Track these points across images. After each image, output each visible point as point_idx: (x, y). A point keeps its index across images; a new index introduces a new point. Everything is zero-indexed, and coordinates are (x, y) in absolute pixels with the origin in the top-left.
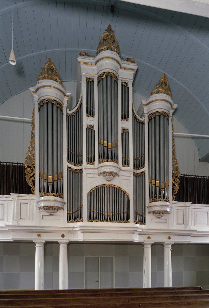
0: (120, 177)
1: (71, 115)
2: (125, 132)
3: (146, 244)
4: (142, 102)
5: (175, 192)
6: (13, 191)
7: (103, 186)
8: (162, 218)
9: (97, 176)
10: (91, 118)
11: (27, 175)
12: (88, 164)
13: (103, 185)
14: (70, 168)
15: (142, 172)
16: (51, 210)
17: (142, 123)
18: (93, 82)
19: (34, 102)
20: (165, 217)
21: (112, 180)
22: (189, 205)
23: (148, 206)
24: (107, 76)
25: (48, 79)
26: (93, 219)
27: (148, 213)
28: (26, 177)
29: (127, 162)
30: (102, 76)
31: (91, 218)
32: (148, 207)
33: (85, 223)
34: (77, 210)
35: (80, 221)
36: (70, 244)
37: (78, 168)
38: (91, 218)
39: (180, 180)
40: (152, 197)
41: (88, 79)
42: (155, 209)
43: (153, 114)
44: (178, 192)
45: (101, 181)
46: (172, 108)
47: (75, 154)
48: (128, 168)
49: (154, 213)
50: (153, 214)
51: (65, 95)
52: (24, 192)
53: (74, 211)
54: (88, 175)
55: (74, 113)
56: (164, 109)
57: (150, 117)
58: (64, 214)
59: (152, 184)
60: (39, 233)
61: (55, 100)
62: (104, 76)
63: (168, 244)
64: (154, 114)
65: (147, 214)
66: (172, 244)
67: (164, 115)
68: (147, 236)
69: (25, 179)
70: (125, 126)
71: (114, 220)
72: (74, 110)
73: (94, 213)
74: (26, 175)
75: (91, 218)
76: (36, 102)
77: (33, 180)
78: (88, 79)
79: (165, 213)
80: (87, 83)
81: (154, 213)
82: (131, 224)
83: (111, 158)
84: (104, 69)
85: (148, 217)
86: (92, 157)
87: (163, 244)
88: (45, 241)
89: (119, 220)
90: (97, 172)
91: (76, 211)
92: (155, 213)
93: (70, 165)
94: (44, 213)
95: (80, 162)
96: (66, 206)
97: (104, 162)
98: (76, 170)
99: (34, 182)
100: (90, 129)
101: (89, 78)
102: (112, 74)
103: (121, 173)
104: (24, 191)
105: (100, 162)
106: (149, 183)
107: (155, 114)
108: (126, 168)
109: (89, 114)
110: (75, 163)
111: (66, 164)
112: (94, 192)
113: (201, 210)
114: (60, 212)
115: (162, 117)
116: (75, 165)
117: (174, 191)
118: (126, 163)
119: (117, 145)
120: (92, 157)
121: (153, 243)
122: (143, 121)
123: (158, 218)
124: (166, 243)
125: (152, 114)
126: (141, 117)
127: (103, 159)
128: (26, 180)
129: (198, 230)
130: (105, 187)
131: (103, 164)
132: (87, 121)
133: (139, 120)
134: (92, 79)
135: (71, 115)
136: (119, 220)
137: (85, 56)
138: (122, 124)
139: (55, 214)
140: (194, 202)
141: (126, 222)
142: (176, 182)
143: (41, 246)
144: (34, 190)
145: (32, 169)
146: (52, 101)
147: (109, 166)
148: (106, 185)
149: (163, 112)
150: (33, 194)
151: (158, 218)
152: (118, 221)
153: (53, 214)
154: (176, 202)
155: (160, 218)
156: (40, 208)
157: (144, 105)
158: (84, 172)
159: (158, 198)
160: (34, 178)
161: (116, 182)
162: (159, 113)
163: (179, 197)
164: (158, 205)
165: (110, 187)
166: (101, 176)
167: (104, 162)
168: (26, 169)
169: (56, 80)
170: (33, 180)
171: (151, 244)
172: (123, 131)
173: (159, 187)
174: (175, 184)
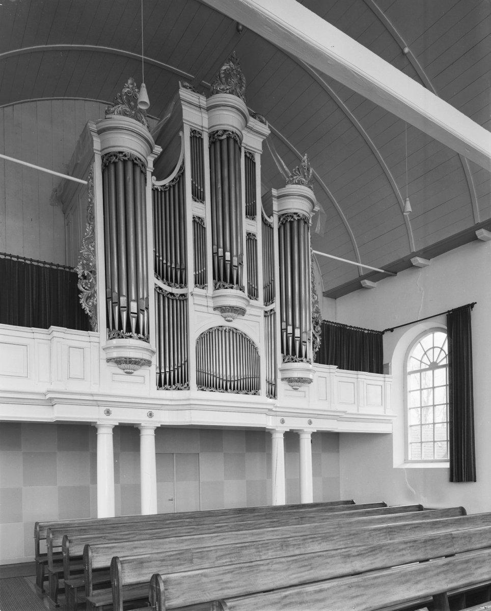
0: (246, 317)
1: (160, 190)
2: (251, 239)
3: (103, 426)
4: (89, 124)
5: (316, 348)
6: (320, 360)
7: (219, 329)
8: (300, 389)
9: (211, 310)
10: (199, 205)
11: (82, 292)
12: (196, 286)
13: (220, 326)
14: (160, 289)
15: (271, 310)
16: (128, 364)
17: (270, 225)
18: (201, 140)
19: (94, 151)
20: (304, 388)
21: (234, 321)
22: (334, 371)
23: (282, 369)
24: (228, 138)
25: (132, 117)
26: (205, 386)
27: (280, 380)
28: (80, 296)
29: (254, 291)
30: (219, 136)
31: (201, 385)
32: (281, 370)
33: (194, 393)
34: (178, 367)
35: (183, 387)
36: (162, 432)
37: (177, 291)
38: (201, 385)
39: (322, 329)
40: (114, 327)
41: (193, 132)
42: (296, 375)
43: (288, 216)
44: (319, 348)
45: (217, 320)
46: (313, 211)
47: (169, 264)
48: (255, 301)
49: (290, 380)
50: (287, 383)
51: (152, 152)
52: (375, 368)
53: (172, 369)
54: (198, 308)
55: (166, 188)
56: (139, 153)
57: (107, 160)
58: (150, 374)
59: (287, 331)
60: (108, 408)
61: (139, 159)
62: (224, 137)
63: (306, 433)
64: (291, 216)
65: (279, 381)
66: (313, 433)
67: (305, 221)
68: (279, 418)
69: (79, 301)
70: (252, 230)
71: (237, 389)
72: (166, 182)
73: (209, 376)
74: (80, 292)
75: (204, 384)
76: (97, 152)
77: (93, 303)
78: (193, 131)
79: (308, 381)
80: (213, 147)
81: (290, 380)
82: (262, 397)
83: (224, 280)
84: (218, 125)
85: (282, 387)
86: (201, 276)
87: (139, 428)
88: (290, 430)
89: (243, 389)
90: (211, 303)
91: (176, 367)
92: (120, 361)
93: (160, 284)
94: (115, 369)
95: (182, 282)
96: (156, 356)
97: (227, 288)
98: (172, 294)
99: (95, 307)
100: (198, 223)
101: (194, 130)
102: (237, 136)
103: (249, 310)
104: (375, 365)
105: (216, 288)
106: (107, 298)
107: (292, 217)
108: (253, 302)
109: (249, 215)
110: (167, 279)
111: (153, 281)
112: (207, 337)
113: (373, 382)
114: (143, 371)
115: (130, 166)
116: (169, 285)
117: (315, 346)
118: (253, 294)
119: (241, 262)
120: (201, 276)
121: (118, 424)
122: (272, 223)
123: (127, 373)
124: (305, 430)
125: (109, 155)
126: (269, 217)
127: (222, 283)
128: (81, 302)
129: (349, 412)
130: (222, 331)
131: (222, 291)
132: (193, 209)
133: (266, 220)
134: (200, 134)
135: (160, 190)
136: (243, 389)
137: (189, 90)
138: (254, 227)
139: (135, 373)
140: (341, 367)
141: (255, 394)
142: (317, 332)
143: (108, 434)
144: (97, 323)
145: (90, 281)
146: (134, 159)
147: (232, 297)
148: (224, 329)
149: (304, 215)
150: (91, 330)
151: (127, 373)
152: (229, 390)
153: (132, 373)
154: (317, 364)
155: (132, 373)
156: (109, 360)
157: (275, 197)
158: (191, 300)
159: (297, 357)
160: (96, 301)
161: (239, 323)
162: (125, 156)
163: (321, 358)
164: (298, 369)
165: (229, 332)
166: (217, 312)
167: (225, 288)
168: (79, 280)
169: (143, 123)
170: (93, 303)
171: (114, 426)
172: (248, 237)
173: (292, 335)
174: (316, 336)
